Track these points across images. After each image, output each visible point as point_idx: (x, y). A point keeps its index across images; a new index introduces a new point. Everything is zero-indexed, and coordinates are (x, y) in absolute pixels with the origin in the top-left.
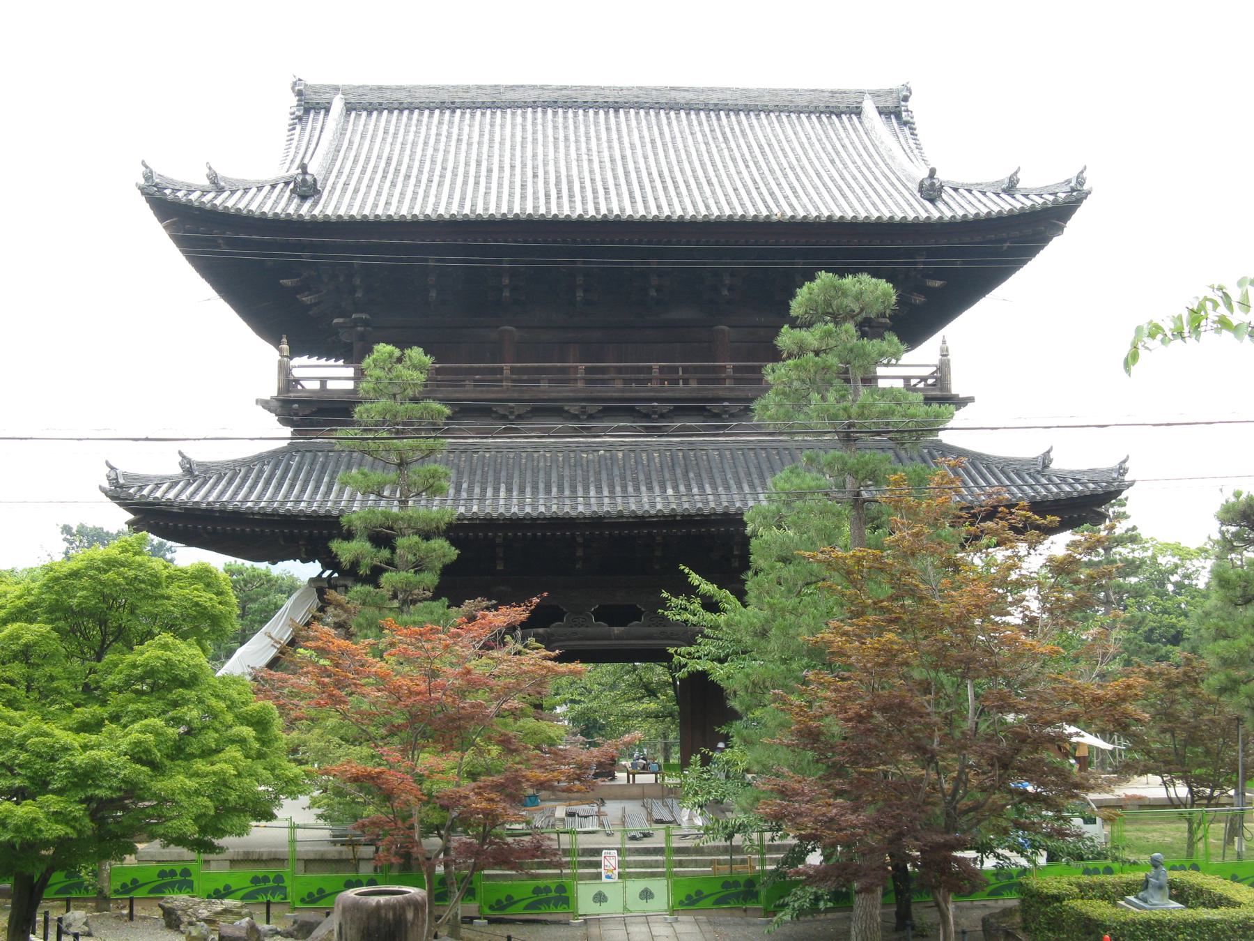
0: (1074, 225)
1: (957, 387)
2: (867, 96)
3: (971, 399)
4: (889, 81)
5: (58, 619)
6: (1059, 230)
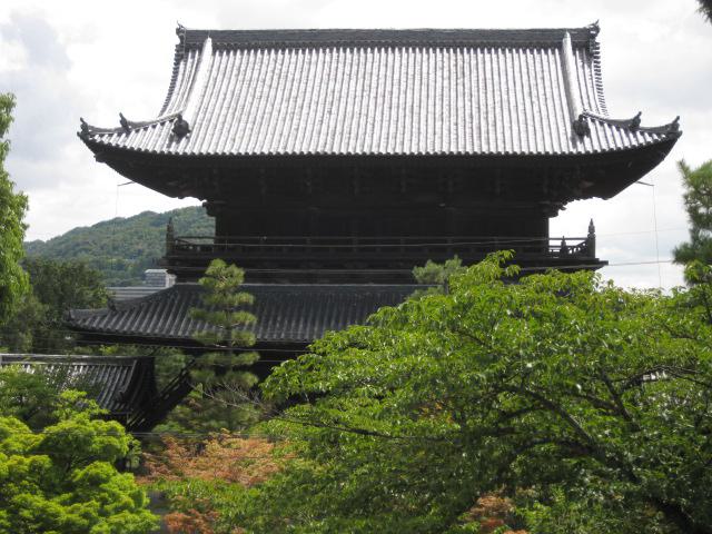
1: (599, 254)
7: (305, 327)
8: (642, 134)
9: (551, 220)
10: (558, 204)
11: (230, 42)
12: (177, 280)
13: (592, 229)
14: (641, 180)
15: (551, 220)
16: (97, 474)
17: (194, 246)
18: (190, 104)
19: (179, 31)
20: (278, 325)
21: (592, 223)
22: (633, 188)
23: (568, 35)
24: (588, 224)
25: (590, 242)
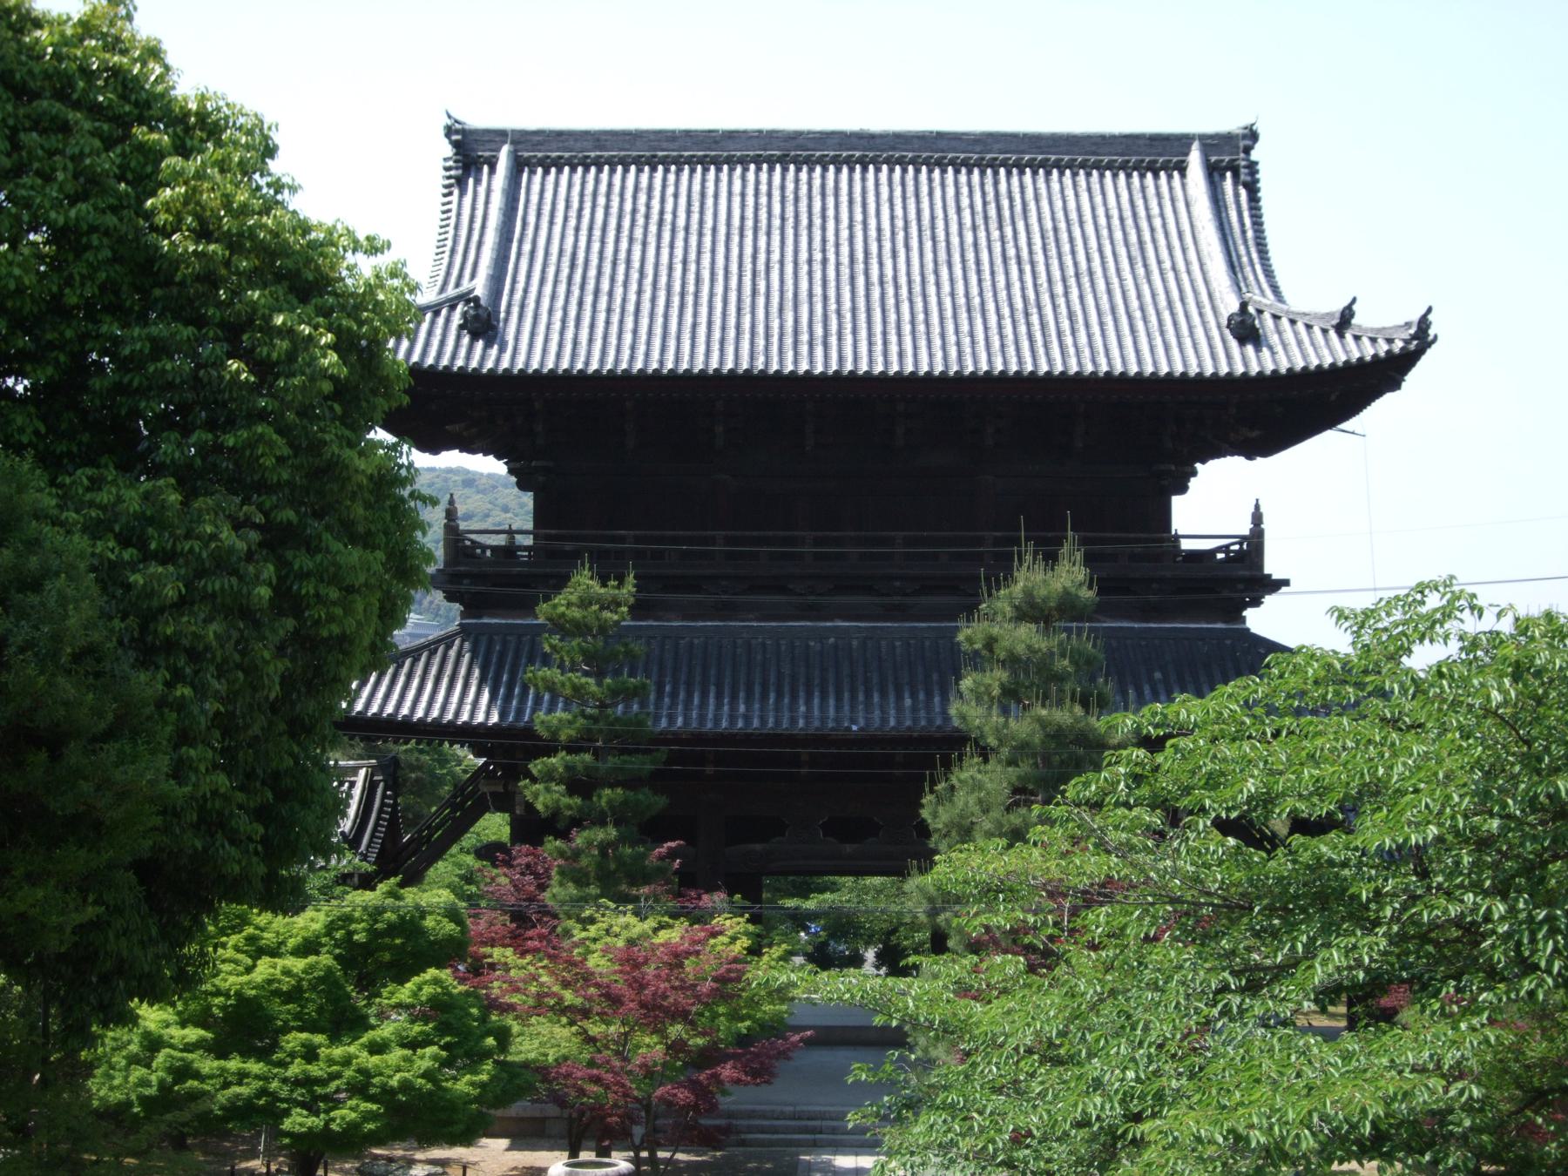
0: (1412, 378)
1: (1273, 566)
2: (1195, 146)
3: (1286, 583)
4: (1227, 122)
5: (1061, 691)
6: (1394, 384)
7: (719, 706)
8: (1357, 338)
9: (1176, 501)
10: (1188, 469)
11: (541, 151)
12: (464, 615)
13: (1257, 518)
14: (1341, 426)
15: (1176, 501)
16: (305, 939)
17: (484, 547)
18: (1195, 210)
19: (449, 132)
20: (667, 700)
21: (1257, 507)
22: (1328, 435)
23: (1195, 146)
24: (1252, 509)
25: (1254, 542)
